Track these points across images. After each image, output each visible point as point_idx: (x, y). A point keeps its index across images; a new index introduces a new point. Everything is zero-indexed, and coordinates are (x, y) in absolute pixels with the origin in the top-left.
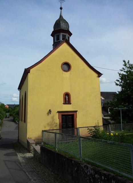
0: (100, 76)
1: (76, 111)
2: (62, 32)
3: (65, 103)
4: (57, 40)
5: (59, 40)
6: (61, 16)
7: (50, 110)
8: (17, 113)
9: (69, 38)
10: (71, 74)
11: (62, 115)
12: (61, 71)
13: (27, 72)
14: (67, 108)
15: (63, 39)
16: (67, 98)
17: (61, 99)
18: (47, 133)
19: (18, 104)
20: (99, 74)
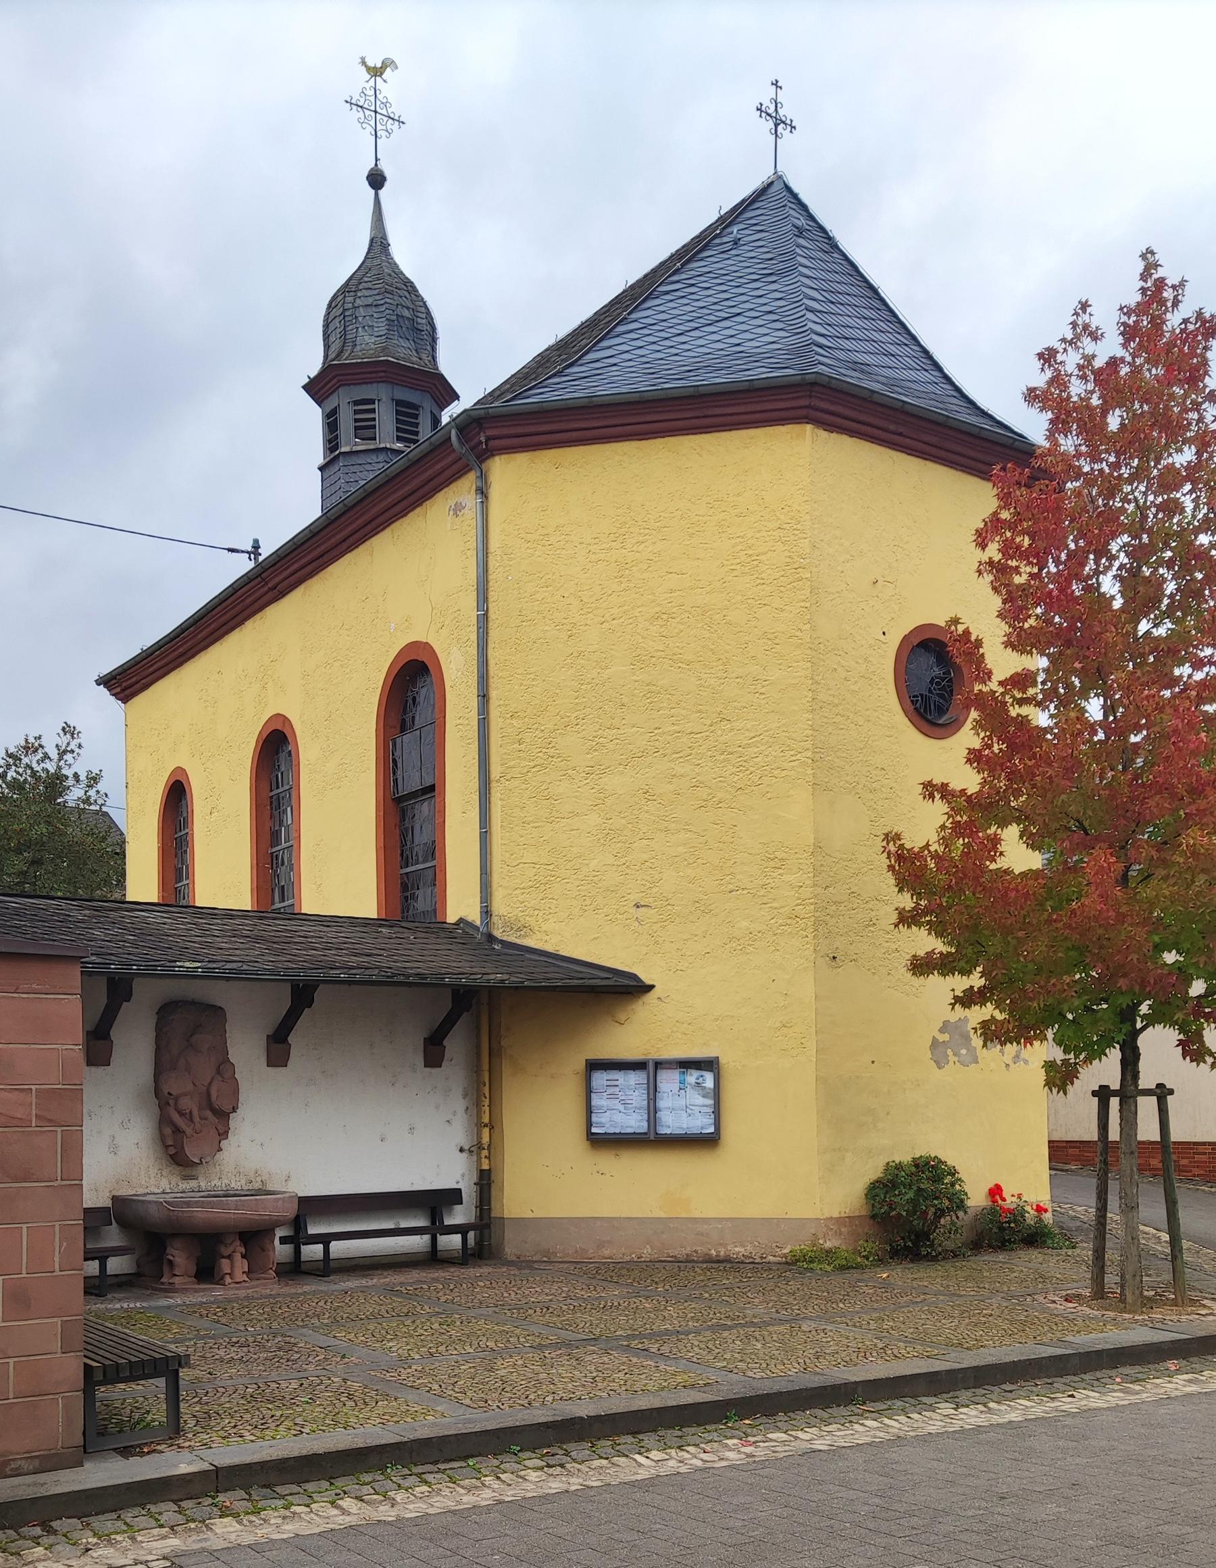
6: (379, 244)
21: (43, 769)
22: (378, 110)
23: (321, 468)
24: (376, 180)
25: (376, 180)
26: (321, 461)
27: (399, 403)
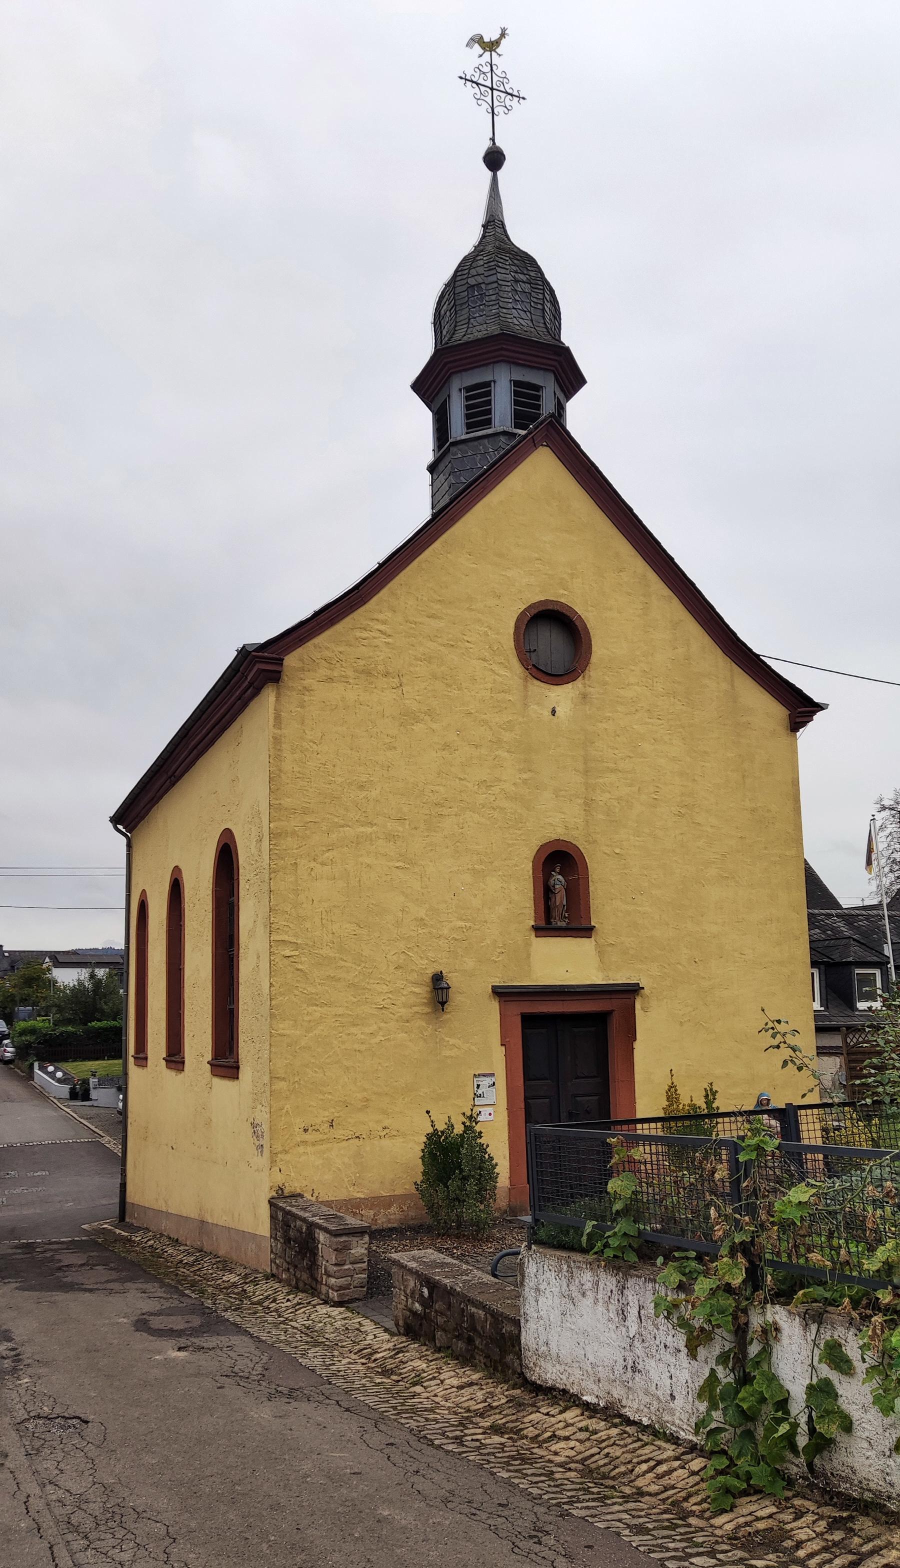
0: (804, 724)
1: (633, 990)
2: (513, 362)
3: (542, 924)
4: (470, 426)
5: (488, 423)
6: (494, 224)
7: (438, 978)
8: (65, 1023)
9: (561, 409)
10: (584, 696)
11: (528, 1020)
12: (512, 671)
13: (255, 671)
14: (565, 964)
15: (520, 419)
16: (561, 888)
17: (519, 895)
18: (87, 1294)
19: (120, 945)
20: (800, 708)
21: (485, 606)
22: (495, 87)
23: (432, 468)
24: (494, 159)
25: (494, 159)
26: (430, 458)
27: (517, 384)
